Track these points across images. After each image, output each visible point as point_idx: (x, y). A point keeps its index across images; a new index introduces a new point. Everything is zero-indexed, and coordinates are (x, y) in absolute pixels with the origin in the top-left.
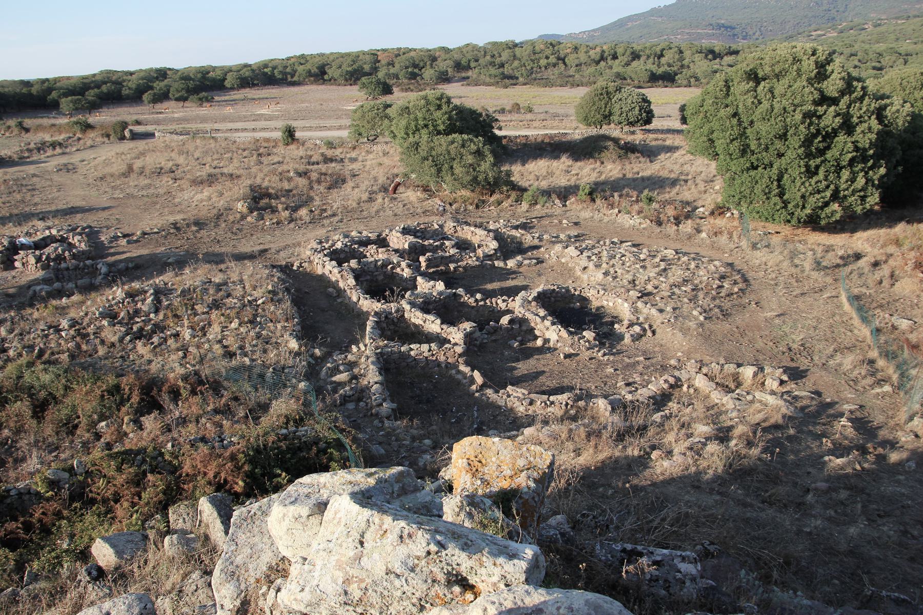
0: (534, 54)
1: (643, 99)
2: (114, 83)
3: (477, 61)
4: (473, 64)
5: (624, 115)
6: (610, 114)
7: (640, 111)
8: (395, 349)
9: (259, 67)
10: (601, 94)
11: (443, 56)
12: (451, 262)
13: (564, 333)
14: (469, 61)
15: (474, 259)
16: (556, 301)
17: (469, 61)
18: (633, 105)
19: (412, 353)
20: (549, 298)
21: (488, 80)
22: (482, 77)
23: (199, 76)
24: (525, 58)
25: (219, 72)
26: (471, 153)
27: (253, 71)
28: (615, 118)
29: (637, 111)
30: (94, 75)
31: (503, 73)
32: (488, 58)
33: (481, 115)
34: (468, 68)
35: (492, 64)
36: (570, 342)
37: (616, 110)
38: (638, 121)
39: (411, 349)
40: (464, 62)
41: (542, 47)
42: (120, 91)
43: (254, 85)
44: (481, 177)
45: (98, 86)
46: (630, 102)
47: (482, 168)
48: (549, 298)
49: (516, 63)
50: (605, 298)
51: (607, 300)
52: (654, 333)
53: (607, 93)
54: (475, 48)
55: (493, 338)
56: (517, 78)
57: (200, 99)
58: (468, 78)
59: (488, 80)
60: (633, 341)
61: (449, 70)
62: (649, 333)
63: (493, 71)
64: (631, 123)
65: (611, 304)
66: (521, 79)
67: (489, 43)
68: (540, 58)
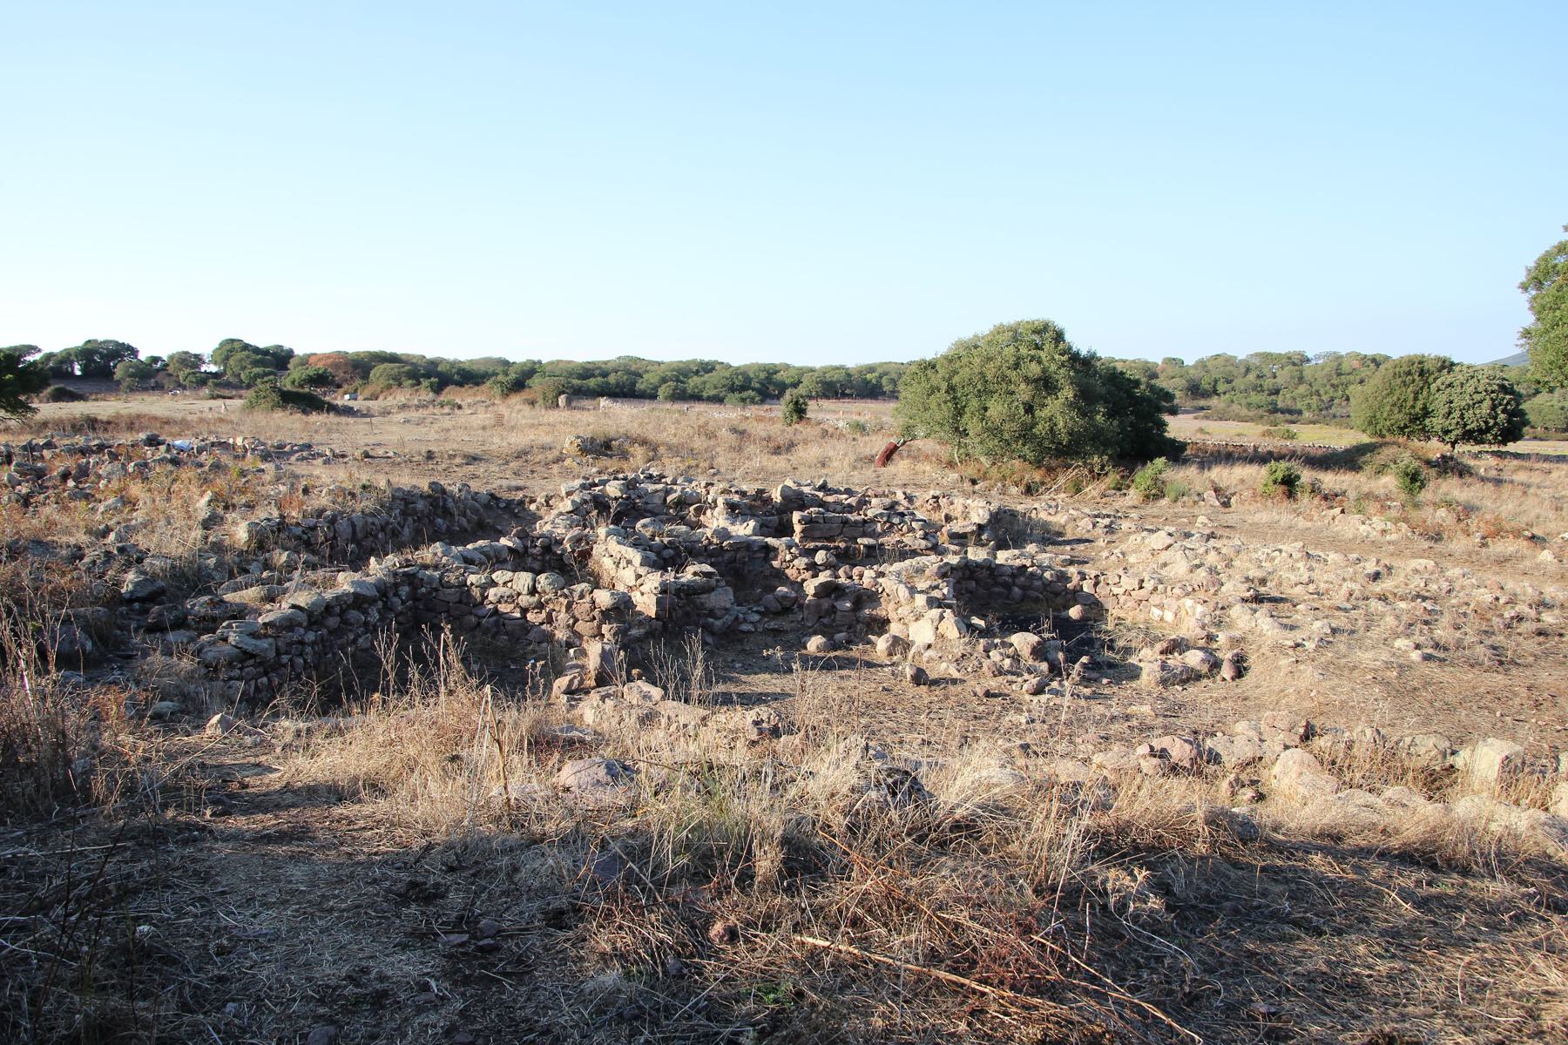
0: (1339, 375)
1: (1502, 387)
2: (629, 372)
3: (1229, 382)
4: (1221, 388)
5: (1456, 414)
6: (1426, 413)
7: (1494, 408)
8: (452, 578)
9: (860, 372)
10: (1409, 373)
11: (1170, 372)
12: (864, 535)
13: (950, 626)
14: (1216, 381)
15: (920, 533)
16: (1024, 598)
17: (1216, 381)
18: (1477, 397)
19: (492, 593)
20: (1008, 587)
21: (1244, 412)
22: (1235, 407)
23: (763, 375)
24: (1320, 381)
25: (793, 373)
26: (1027, 380)
27: (849, 375)
28: (1436, 422)
29: (1485, 408)
30: (606, 363)
31: (1274, 404)
32: (1251, 377)
33: (1137, 383)
34: (1206, 395)
35: (1258, 389)
36: (958, 652)
37: (1439, 403)
38: (1488, 429)
39: (494, 584)
40: (1205, 385)
41: (1356, 364)
42: (634, 384)
43: (844, 395)
44: (1041, 429)
45: (605, 375)
46: (1471, 390)
47: (1045, 413)
48: (1008, 587)
49: (1302, 389)
50: (1155, 599)
51: (1161, 607)
52: (1240, 672)
53: (1422, 373)
54: (1229, 361)
55: (773, 625)
56: (1300, 412)
57: (743, 400)
58: (1209, 408)
59: (1244, 412)
60: (1164, 682)
61: (1178, 394)
62: (1227, 671)
63: (1255, 398)
64: (1471, 432)
65: (1169, 616)
66: (1306, 414)
67: (1257, 355)
68: (1350, 383)
